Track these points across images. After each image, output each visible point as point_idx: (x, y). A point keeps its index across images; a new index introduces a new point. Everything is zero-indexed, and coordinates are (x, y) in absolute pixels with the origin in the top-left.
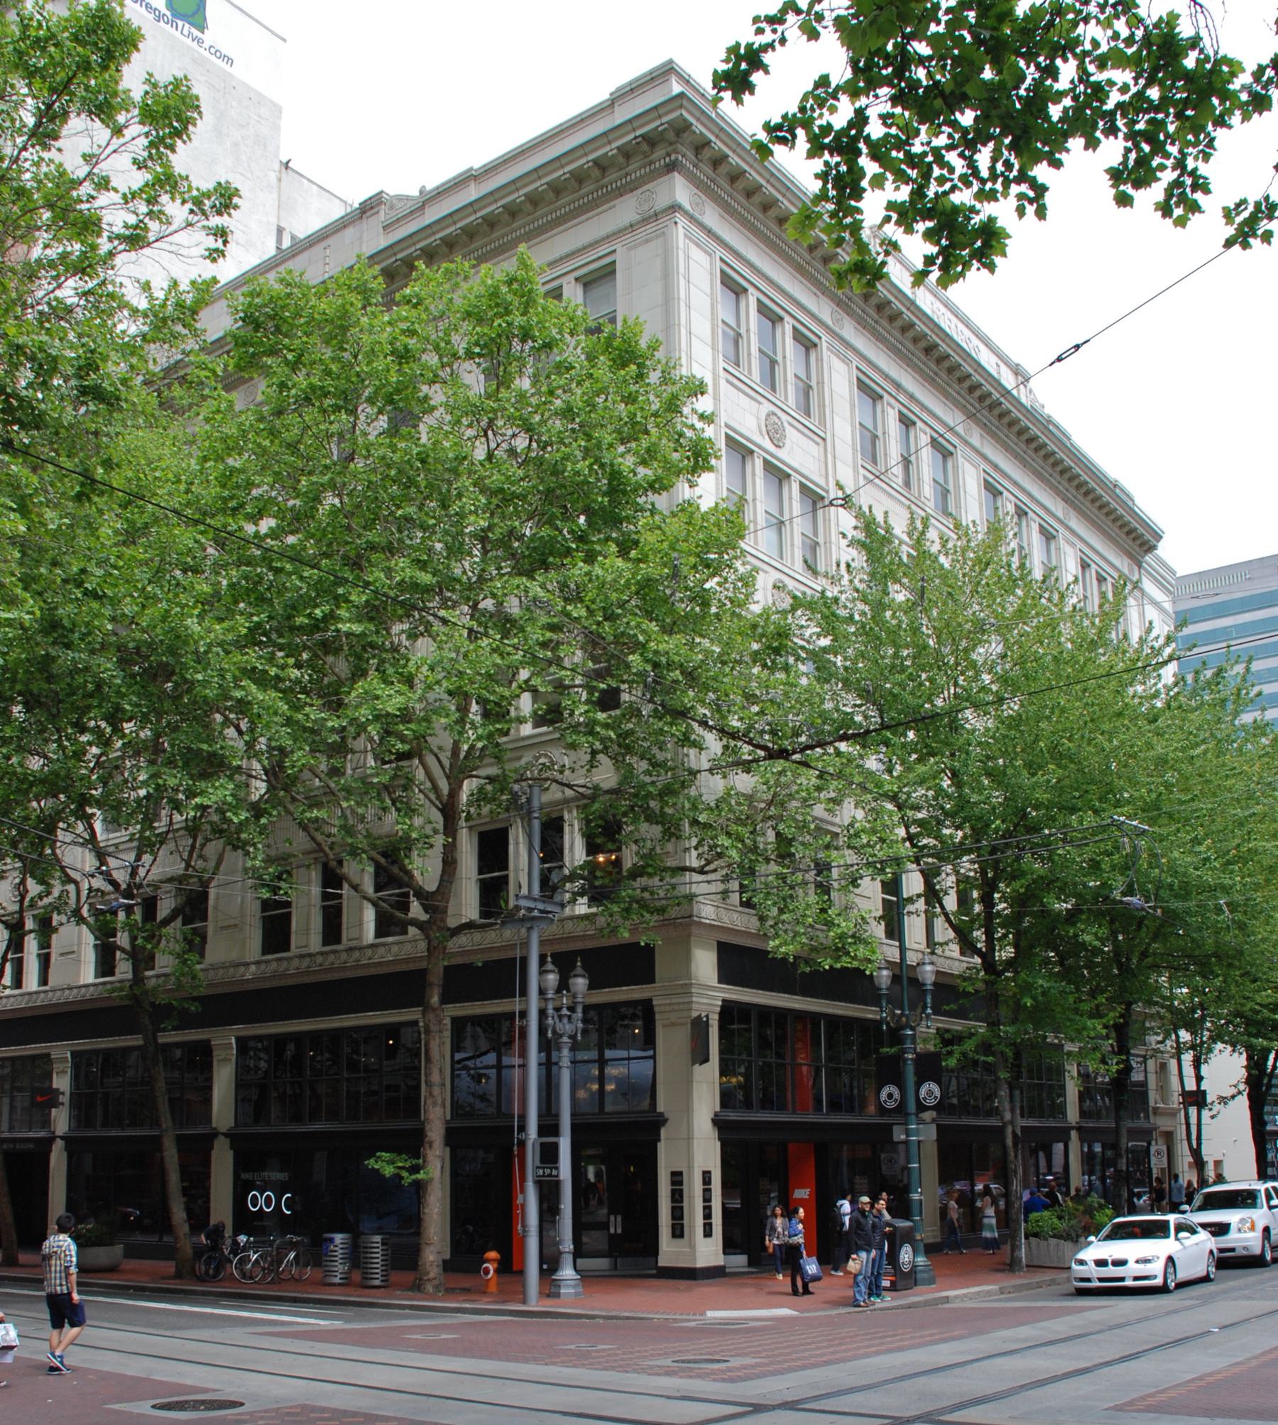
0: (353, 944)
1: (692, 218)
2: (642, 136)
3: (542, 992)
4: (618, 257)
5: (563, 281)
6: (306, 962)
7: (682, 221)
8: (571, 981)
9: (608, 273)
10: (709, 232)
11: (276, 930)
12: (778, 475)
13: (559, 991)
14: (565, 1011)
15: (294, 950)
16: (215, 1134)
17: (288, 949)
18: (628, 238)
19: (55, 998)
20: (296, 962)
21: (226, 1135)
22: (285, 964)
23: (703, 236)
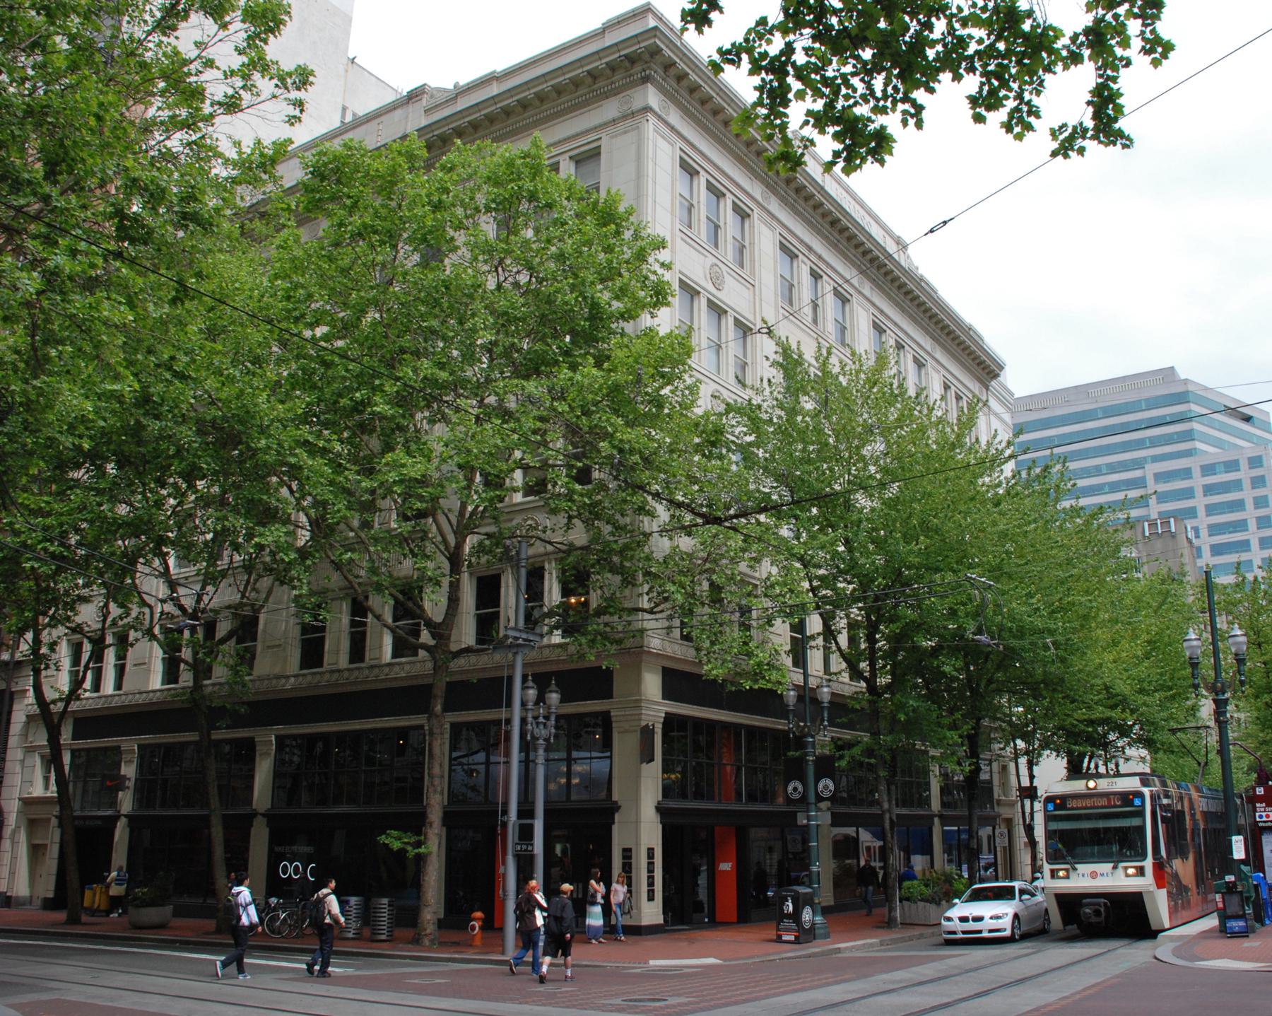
0: (373, 662)
1: (659, 117)
2: (588, 72)
3: (523, 704)
4: (603, 143)
5: (561, 158)
6: (336, 676)
7: (652, 119)
8: (547, 695)
9: (595, 154)
10: (672, 128)
11: (312, 652)
12: (718, 311)
13: (537, 703)
14: (541, 720)
15: (326, 667)
16: (254, 814)
17: (321, 665)
18: (611, 130)
19: (127, 701)
20: (327, 676)
21: (263, 815)
22: (318, 677)
23: (667, 131)
